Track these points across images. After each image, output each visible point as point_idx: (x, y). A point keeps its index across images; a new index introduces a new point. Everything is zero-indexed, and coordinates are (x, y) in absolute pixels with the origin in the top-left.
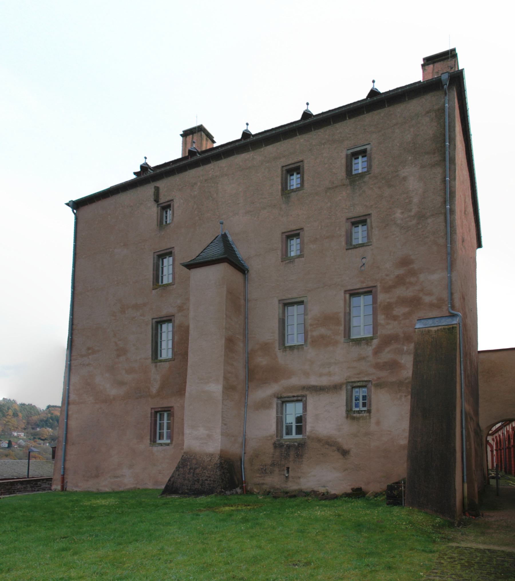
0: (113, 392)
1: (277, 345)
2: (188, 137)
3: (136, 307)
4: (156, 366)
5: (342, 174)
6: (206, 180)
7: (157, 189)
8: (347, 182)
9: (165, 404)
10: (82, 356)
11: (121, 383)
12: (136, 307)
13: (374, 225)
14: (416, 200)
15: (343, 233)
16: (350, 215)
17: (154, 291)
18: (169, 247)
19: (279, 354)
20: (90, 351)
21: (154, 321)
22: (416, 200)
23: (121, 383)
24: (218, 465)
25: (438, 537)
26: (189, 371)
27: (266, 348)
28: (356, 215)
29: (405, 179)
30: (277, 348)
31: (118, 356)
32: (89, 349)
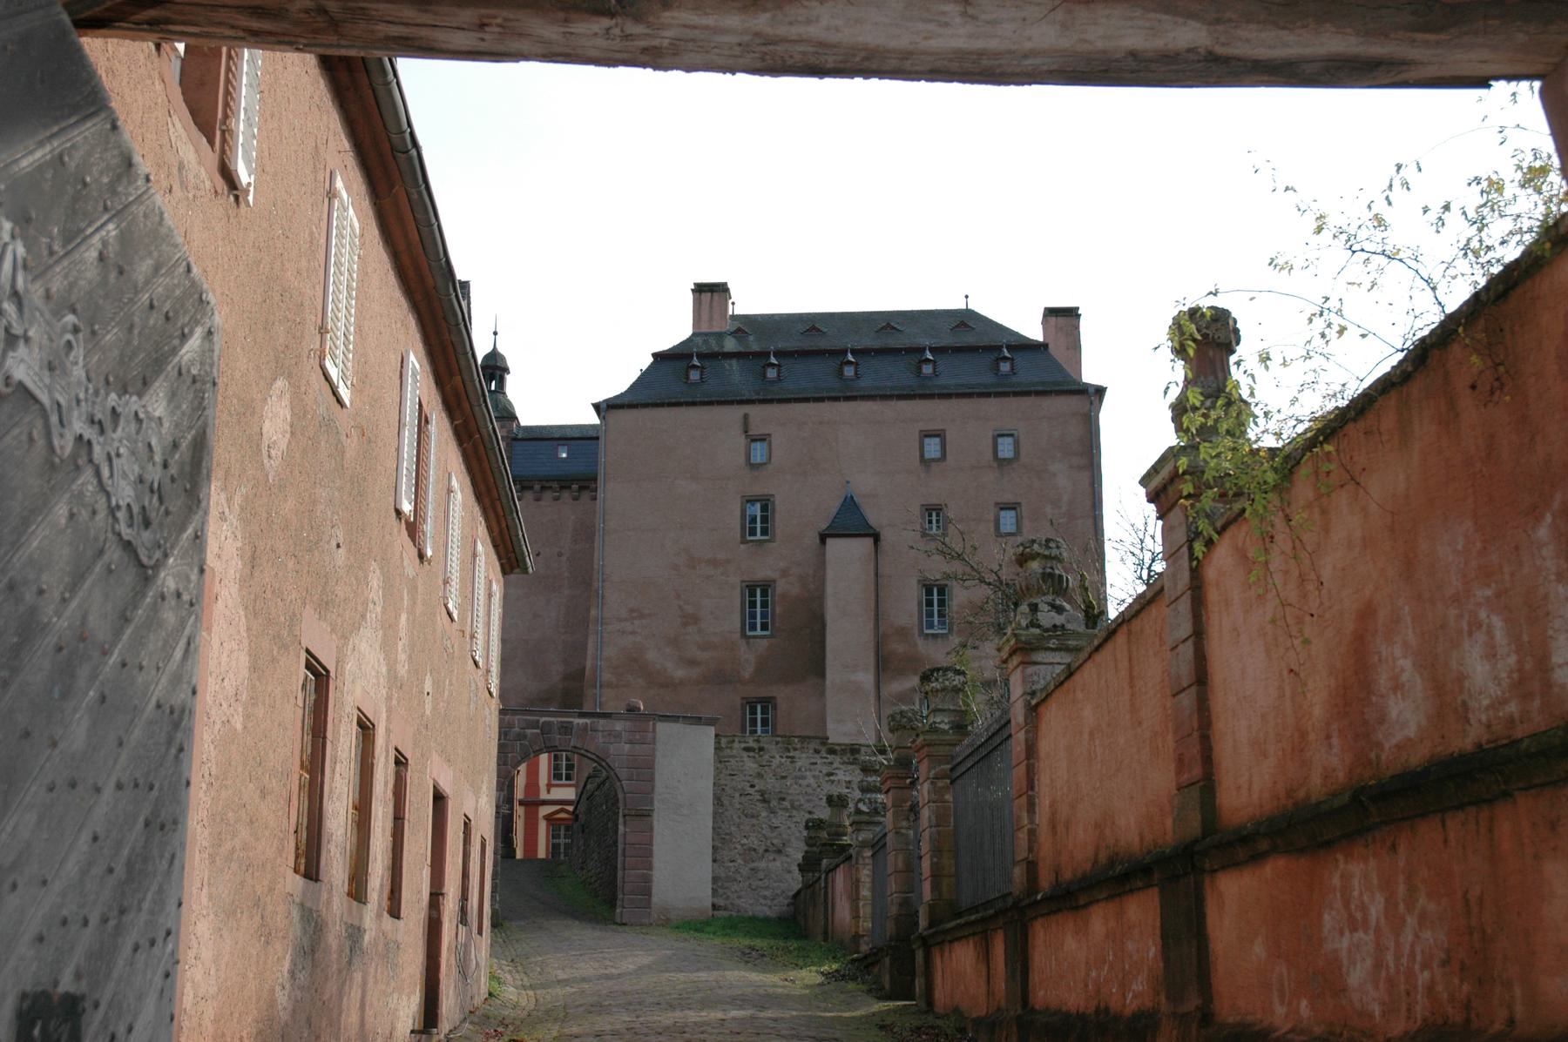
0: (679, 673)
1: (916, 631)
2: (703, 294)
3: (714, 563)
4: (748, 643)
5: (989, 454)
6: (821, 423)
7: (746, 417)
8: (995, 465)
9: (764, 692)
10: (620, 620)
11: (692, 663)
12: (714, 563)
13: (1024, 514)
14: (1065, 498)
15: (992, 519)
16: (999, 500)
17: (742, 546)
18: (770, 493)
19: (920, 642)
20: (635, 615)
21: (744, 584)
22: (1065, 498)
23: (692, 663)
24: (1550, 632)
25: (1301, 526)
26: (829, 656)
27: (903, 633)
28: (1005, 501)
29: (1054, 475)
30: (916, 635)
31: (685, 625)
32: (632, 611)
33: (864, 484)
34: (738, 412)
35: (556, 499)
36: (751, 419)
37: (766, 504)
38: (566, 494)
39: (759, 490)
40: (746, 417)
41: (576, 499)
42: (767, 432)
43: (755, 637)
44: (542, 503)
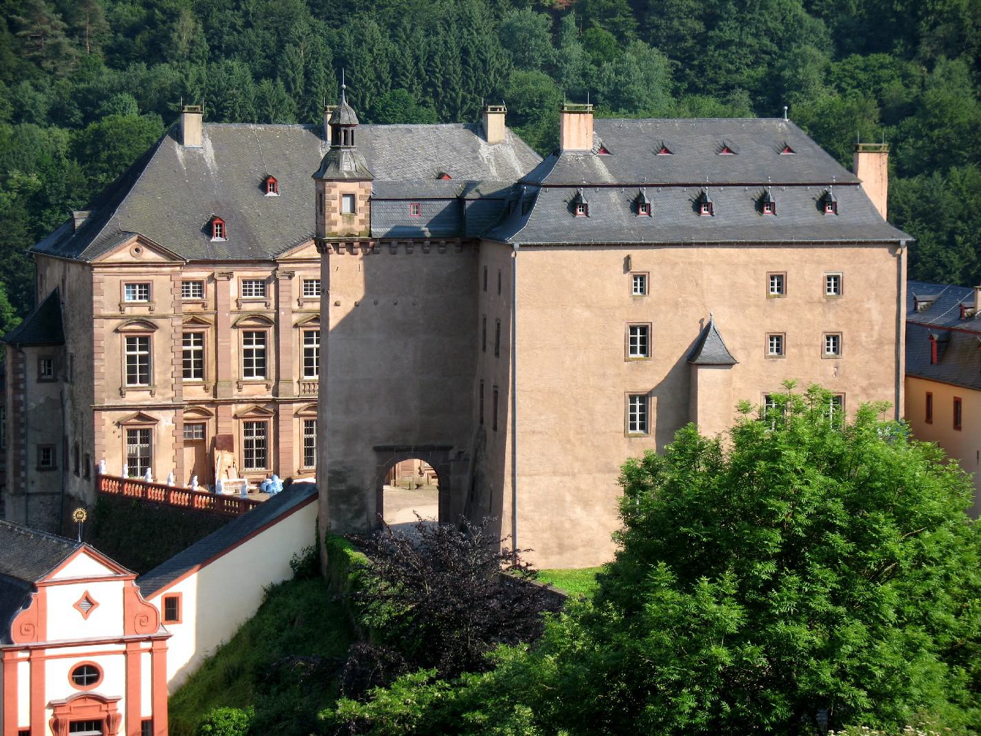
6: (689, 263)
8: (824, 300)
33: (722, 321)
34: (624, 253)
35: (410, 253)
36: (633, 259)
37: (644, 330)
38: (418, 248)
39: (640, 319)
40: (628, 259)
41: (427, 252)
42: (646, 270)
43: (636, 436)
44: (397, 256)
